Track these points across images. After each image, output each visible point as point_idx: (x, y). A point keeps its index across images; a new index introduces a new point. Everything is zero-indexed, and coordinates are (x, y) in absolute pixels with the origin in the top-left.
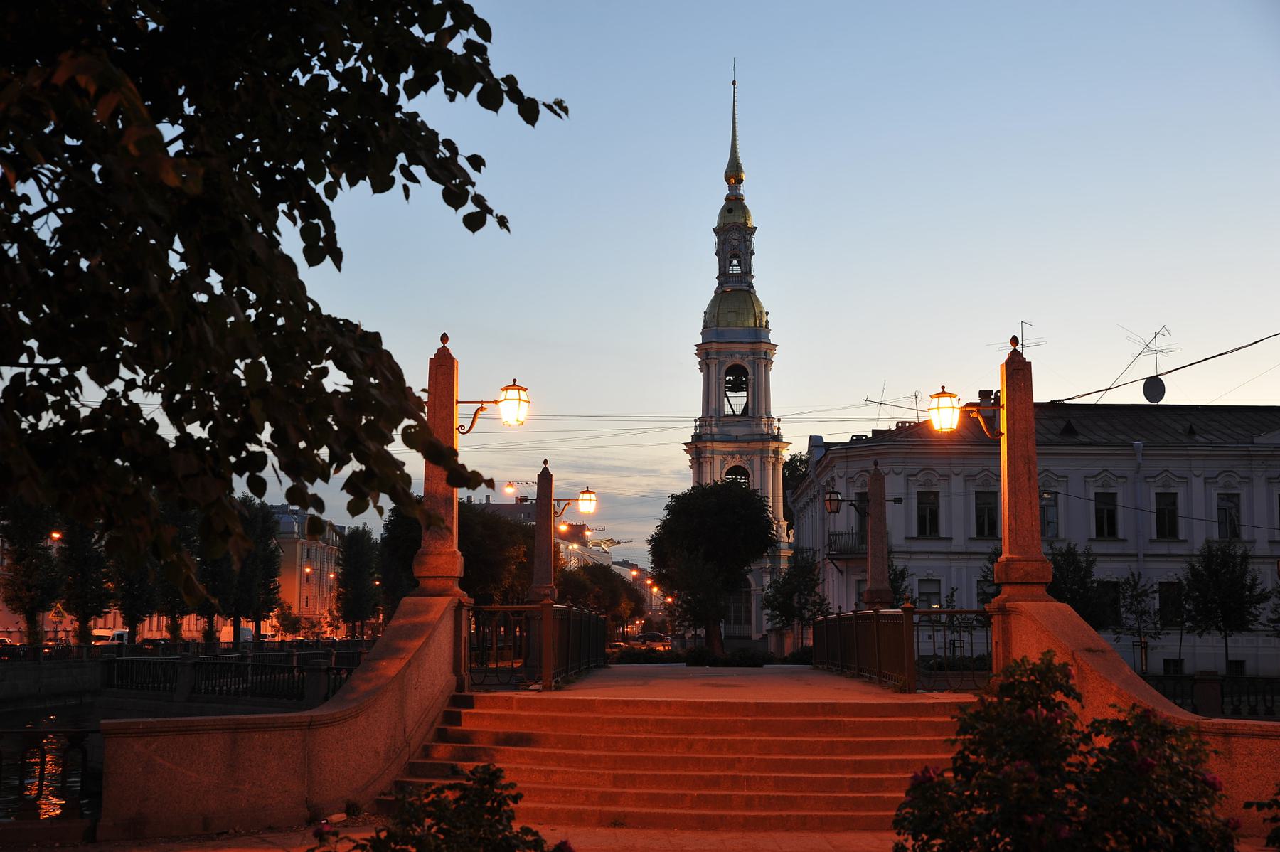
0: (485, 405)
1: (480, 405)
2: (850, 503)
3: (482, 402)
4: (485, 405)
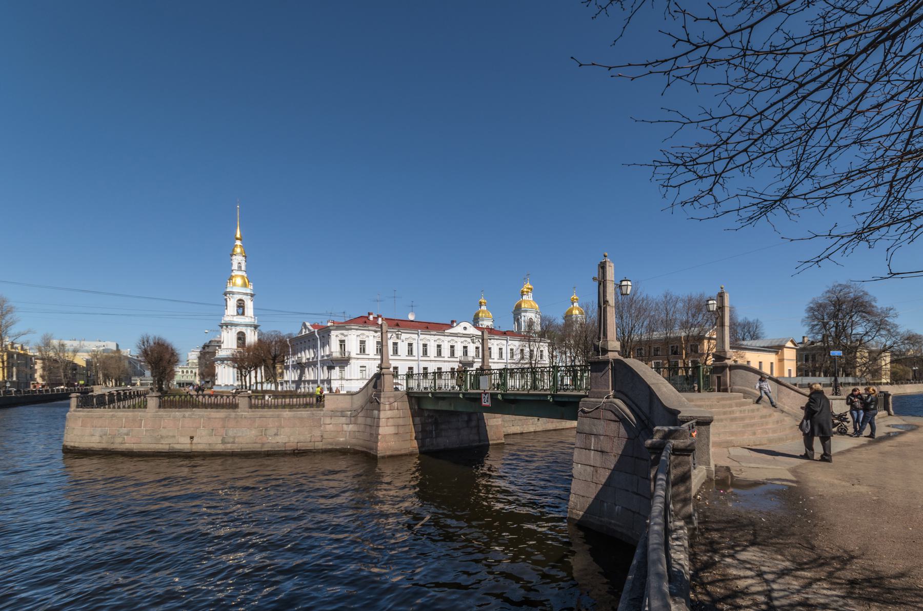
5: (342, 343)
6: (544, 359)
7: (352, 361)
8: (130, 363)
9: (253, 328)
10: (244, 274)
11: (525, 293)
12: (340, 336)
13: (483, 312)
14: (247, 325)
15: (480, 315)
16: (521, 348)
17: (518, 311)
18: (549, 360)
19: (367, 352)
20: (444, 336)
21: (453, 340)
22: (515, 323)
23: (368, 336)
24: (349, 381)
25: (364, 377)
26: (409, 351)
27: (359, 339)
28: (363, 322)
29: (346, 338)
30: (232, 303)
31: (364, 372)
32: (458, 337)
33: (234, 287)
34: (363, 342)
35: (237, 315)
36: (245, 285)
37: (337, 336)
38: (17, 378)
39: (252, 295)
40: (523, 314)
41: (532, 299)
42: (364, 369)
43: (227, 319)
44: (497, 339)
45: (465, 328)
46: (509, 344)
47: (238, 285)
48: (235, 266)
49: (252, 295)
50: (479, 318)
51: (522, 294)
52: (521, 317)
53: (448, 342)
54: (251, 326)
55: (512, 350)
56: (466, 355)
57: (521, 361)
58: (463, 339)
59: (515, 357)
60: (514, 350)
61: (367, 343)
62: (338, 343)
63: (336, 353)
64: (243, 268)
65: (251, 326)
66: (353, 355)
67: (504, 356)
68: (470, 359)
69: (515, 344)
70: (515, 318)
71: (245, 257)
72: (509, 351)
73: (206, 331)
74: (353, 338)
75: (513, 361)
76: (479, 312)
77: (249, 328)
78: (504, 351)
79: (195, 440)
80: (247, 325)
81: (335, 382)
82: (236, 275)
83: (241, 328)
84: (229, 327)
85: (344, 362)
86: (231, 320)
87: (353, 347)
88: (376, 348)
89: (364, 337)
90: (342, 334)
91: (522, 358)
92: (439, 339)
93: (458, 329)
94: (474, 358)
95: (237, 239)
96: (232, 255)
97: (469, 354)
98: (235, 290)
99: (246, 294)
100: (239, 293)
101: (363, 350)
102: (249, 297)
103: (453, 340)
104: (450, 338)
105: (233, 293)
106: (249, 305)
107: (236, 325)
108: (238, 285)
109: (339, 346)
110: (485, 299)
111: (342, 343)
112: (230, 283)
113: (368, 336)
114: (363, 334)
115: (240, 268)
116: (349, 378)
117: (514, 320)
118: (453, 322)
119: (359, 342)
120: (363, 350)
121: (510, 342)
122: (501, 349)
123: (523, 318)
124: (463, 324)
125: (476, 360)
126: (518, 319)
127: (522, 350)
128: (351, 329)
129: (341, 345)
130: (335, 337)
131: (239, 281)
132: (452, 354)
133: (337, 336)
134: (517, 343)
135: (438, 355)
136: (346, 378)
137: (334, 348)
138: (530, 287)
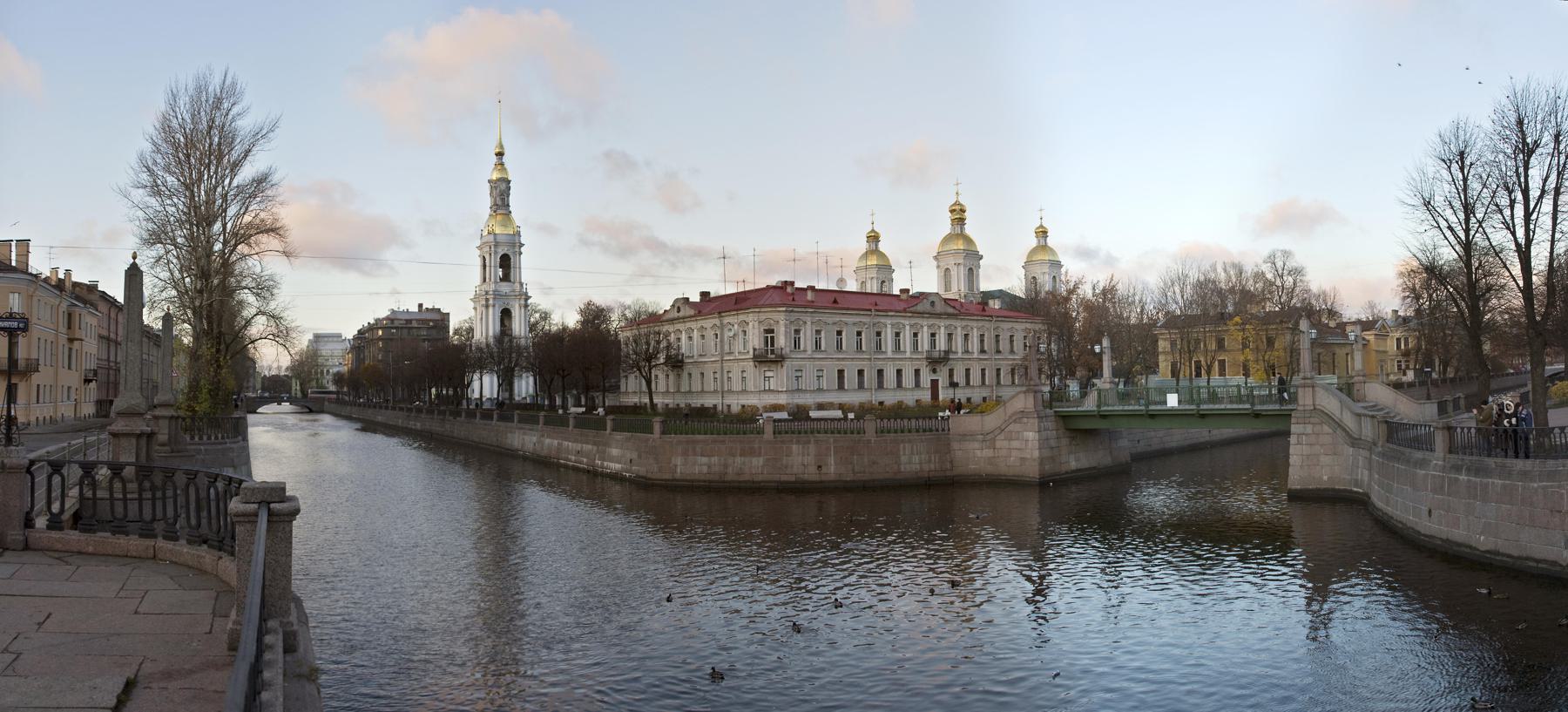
79: (824, 470)
116: (780, 390)
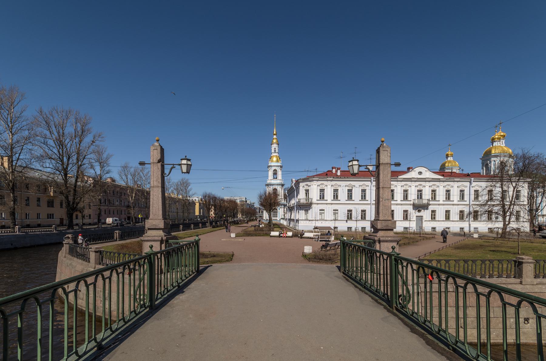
0: (175, 166)
1: (172, 166)
2: (365, 167)
3: (173, 165)
4: (175, 166)
5: (307, 191)
6: (522, 199)
7: (314, 206)
8: (249, 206)
9: (281, 186)
10: (277, 154)
11: (496, 140)
12: (305, 187)
13: (450, 162)
14: (278, 185)
15: (447, 165)
16: (488, 189)
17: (487, 156)
18: (527, 201)
19: (325, 199)
20: (397, 181)
21: (406, 185)
22: (483, 169)
23: (410, 186)
24: (311, 222)
25: (323, 218)
26: (362, 196)
27: (319, 188)
28: (327, 175)
29: (309, 188)
30: (271, 173)
31: (323, 214)
32: (411, 181)
33: (272, 163)
34: (322, 191)
35: (273, 179)
36: (277, 161)
37: (303, 187)
38: (203, 214)
39: (281, 167)
40: (493, 159)
41: (504, 145)
42: (323, 212)
43: (268, 182)
44: (458, 181)
45: (420, 173)
46: (472, 185)
47: (274, 162)
48: (273, 151)
49: (281, 167)
50: (445, 168)
51: (493, 141)
52: (490, 162)
53: (415, 186)
54: (280, 185)
55: (476, 191)
56: (421, 198)
57: (489, 203)
58: (417, 183)
59: (480, 199)
60: (480, 191)
61: (325, 190)
62: (304, 192)
63: (303, 201)
64: (277, 151)
65: (280, 185)
66: (314, 201)
67: (466, 198)
68: (425, 202)
69: (482, 185)
70: (483, 164)
71: (278, 144)
72: (473, 193)
73: (223, 188)
74: (314, 188)
75: (477, 203)
76: (445, 163)
77: (279, 186)
78: (466, 193)
80: (278, 185)
81: (302, 222)
82: (273, 156)
83: (275, 186)
84: (269, 186)
85: (306, 207)
86: (270, 182)
87: (314, 195)
88: (319, 194)
89: (324, 186)
90: (307, 185)
91: (491, 199)
92: (434, 185)
93: (413, 174)
94: (429, 200)
95: (274, 135)
96: (271, 144)
97: (423, 197)
98: (272, 164)
99: (278, 166)
100: (274, 166)
101: (322, 197)
102: (280, 168)
103: (420, 185)
104: (403, 183)
105: (271, 166)
106: (279, 173)
107: (273, 185)
108: (274, 162)
109: (304, 195)
110: (451, 151)
111: (307, 191)
112: (270, 160)
113: (410, 186)
114: (322, 184)
115: (275, 151)
116: (311, 219)
117: (483, 166)
118: (409, 169)
119: (319, 191)
120: (322, 197)
121: (474, 184)
122: (462, 191)
123: (493, 163)
124: (418, 170)
125: (431, 203)
126: (487, 164)
127: (490, 192)
128: (313, 181)
129: (306, 193)
130: (302, 187)
131: (275, 159)
132: (406, 197)
133: (303, 187)
134: (484, 184)
135: (404, 199)
136: (309, 219)
137: (302, 195)
138: (502, 134)
